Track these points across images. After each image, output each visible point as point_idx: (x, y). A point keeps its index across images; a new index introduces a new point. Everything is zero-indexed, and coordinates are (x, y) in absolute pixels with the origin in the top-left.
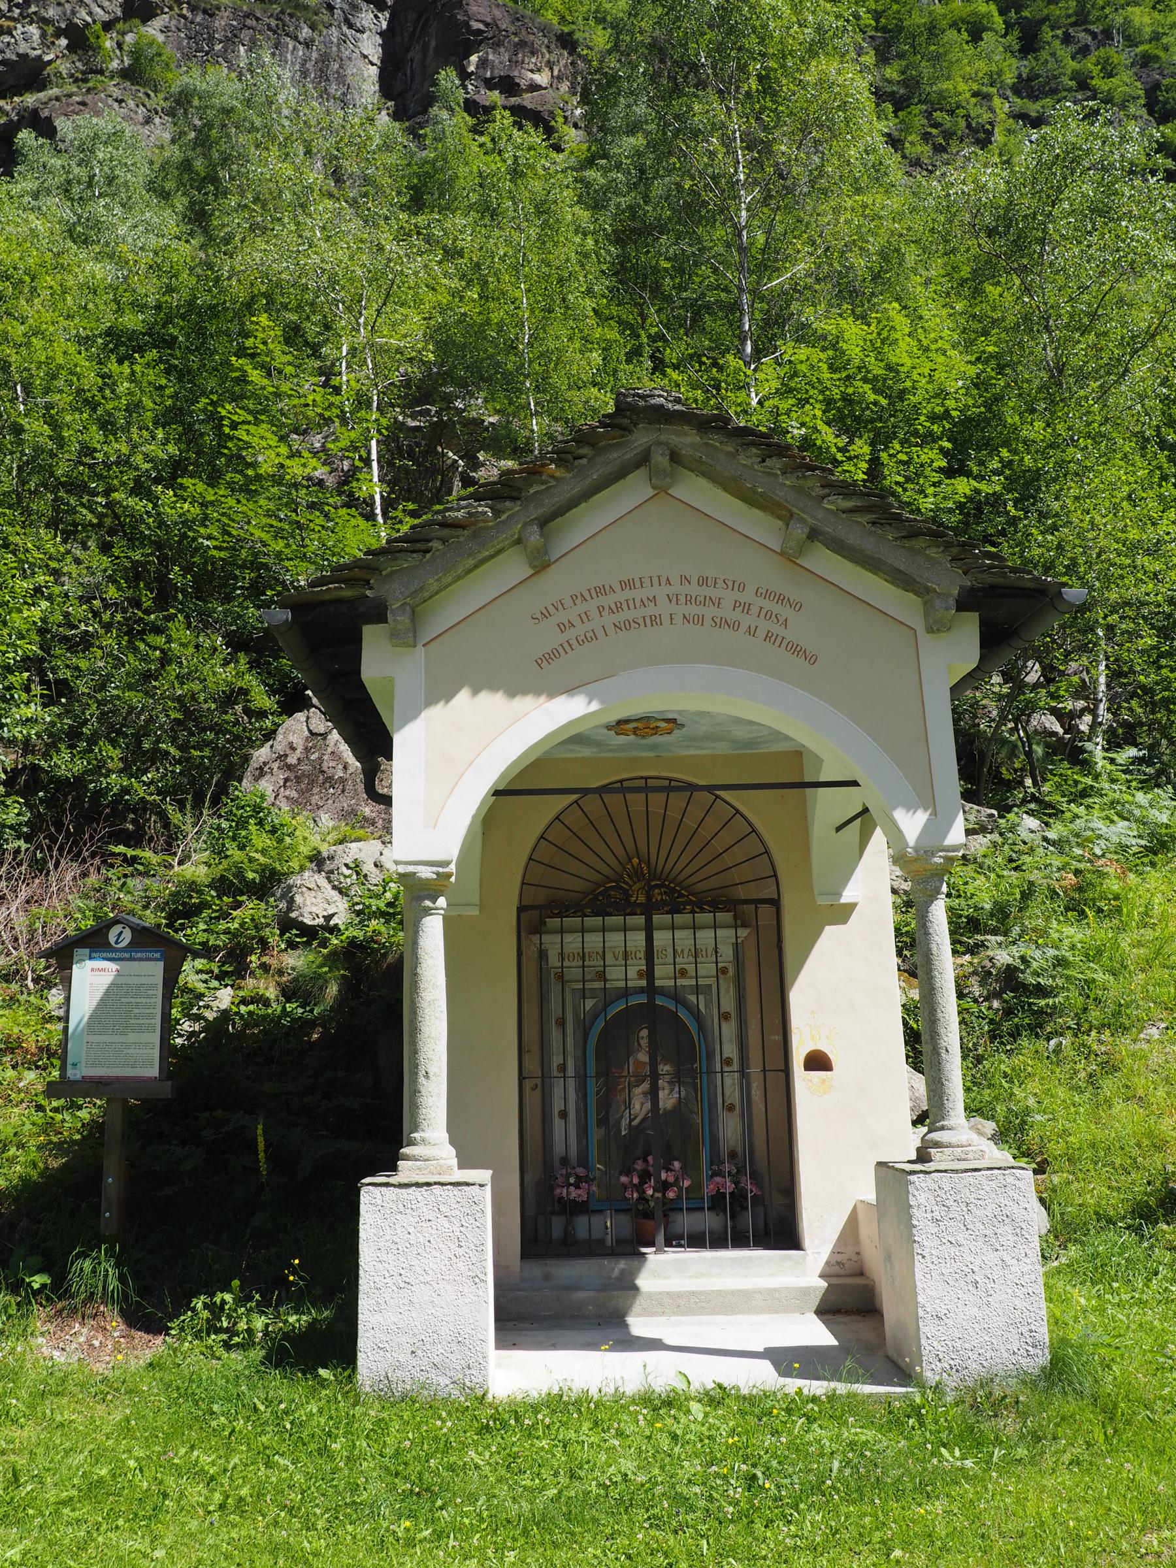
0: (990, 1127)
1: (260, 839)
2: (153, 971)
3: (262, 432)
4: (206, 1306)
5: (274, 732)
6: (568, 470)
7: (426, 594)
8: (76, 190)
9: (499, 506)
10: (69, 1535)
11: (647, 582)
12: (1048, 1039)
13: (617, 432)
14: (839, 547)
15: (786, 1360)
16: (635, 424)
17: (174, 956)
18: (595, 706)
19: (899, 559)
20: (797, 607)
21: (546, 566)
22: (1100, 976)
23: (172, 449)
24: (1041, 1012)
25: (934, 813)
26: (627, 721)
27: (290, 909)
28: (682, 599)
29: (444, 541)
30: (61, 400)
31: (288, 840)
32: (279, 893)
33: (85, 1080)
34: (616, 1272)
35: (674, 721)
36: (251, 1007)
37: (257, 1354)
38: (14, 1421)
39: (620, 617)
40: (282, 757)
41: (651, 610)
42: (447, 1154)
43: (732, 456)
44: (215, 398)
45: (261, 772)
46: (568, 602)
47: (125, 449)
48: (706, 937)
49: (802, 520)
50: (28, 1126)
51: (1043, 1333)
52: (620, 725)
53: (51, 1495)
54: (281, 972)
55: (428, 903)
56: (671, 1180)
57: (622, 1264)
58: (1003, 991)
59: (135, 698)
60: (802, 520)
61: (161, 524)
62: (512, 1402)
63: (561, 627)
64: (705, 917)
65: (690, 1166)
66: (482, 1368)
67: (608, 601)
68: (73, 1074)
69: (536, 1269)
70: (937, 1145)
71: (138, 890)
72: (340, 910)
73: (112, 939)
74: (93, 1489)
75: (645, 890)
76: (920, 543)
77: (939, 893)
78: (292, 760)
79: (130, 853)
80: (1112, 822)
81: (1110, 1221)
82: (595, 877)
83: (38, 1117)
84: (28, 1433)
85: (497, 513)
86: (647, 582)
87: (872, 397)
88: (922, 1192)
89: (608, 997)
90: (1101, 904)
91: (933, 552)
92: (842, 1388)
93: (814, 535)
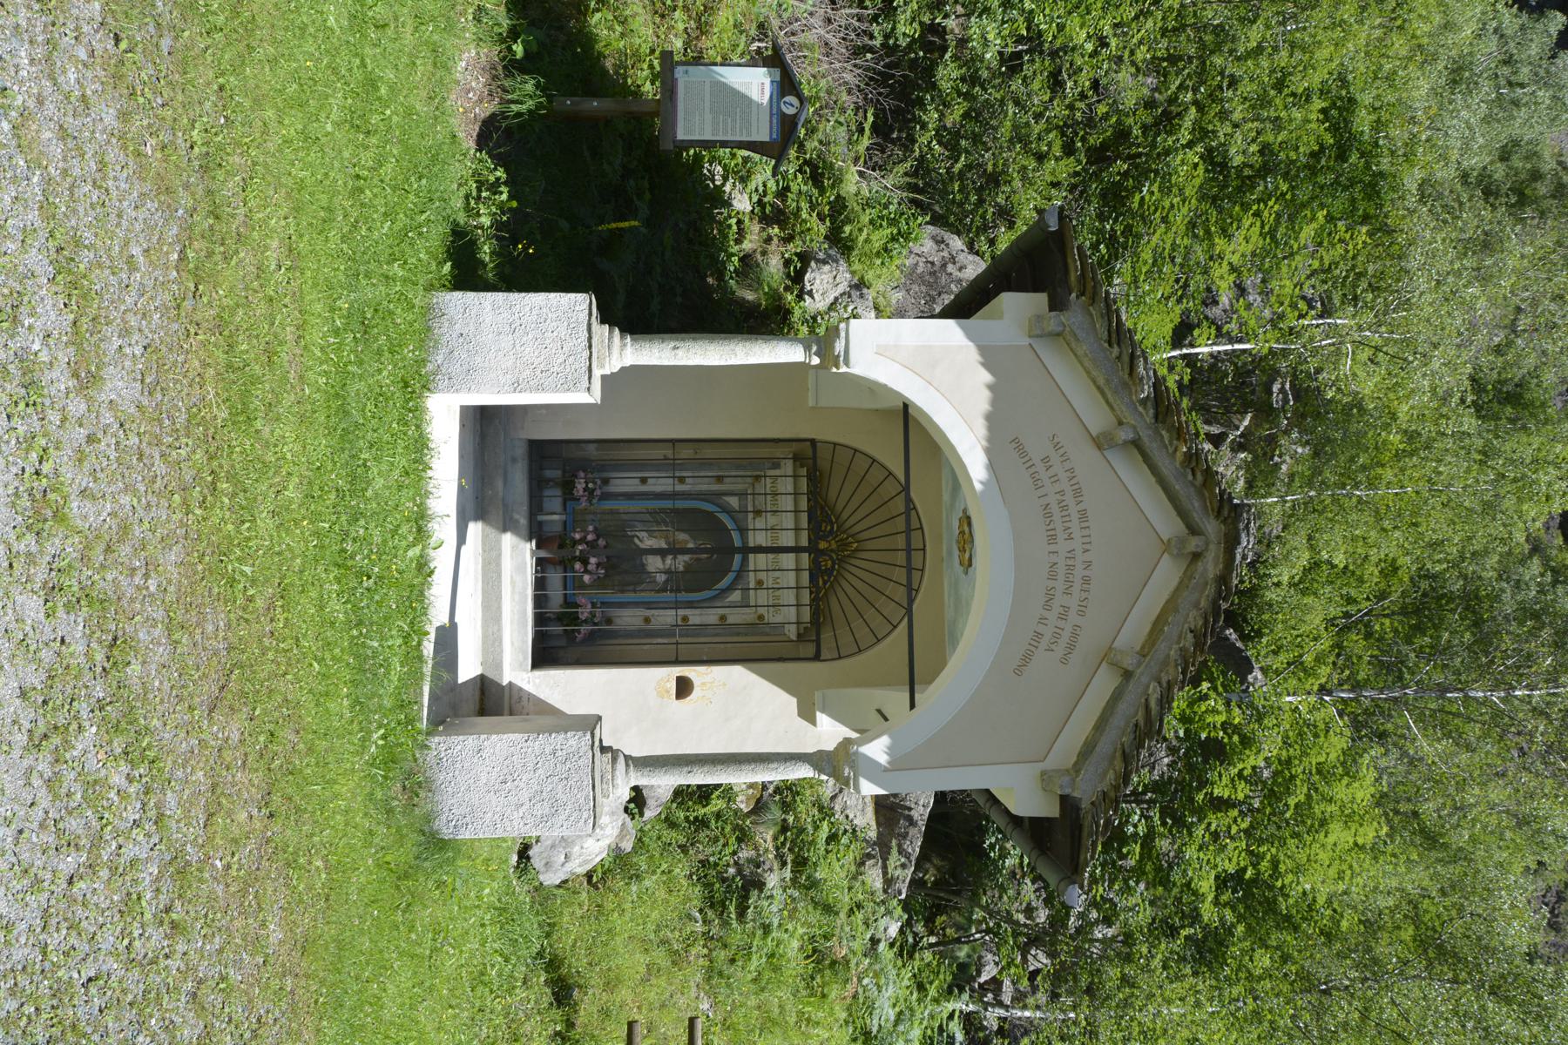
0: (628, 846)
1: (879, 238)
2: (762, 134)
3: (1254, 239)
4: (498, 179)
5: (977, 253)
6: (1182, 463)
7: (1073, 345)
8: (1506, 71)
9: (1149, 404)
10: (342, 62)
11: (1086, 532)
12: (701, 911)
13: (1216, 505)
14: (1116, 697)
15: (448, 638)
16: (1224, 521)
17: (775, 150)
18: (978, 487)
19: (1105, 746)
20: (1064, 661)
21: (1099, 447)
22: (755, 963)
23: (1238, 160)
24: (724, 907)
25: (886, 770)
26: (970, 524)
27: (818, 261)
28: (1070, 562)
29: (1119, 358)
30: (1283, 57)
31: (878, 262)
32: (832, 252)
33: (674, 82)
34: (516, 516)
35: (970, 565)
36: (735, 228)
37: (461, 218)
38: (416, 29)
39: (1055, 508)
40: (953, 260)
41: (1061, 536)
42: (614, 364)
43: (1196, 605)
44: (1288, 197)
45: (939, 242)
46: (1067, 465)
47: (1237, 116)
48: (789, 597)
49: (1139, 664)
50: (638, 41)
51: (465, 835)
52: (967, 520)
53: (368, 51)
54: (764, 253)
55: (814, 348)
56: (590, 567)
57: (523, 521)
58: (743, 877)
59: (1005, 130)
60: (1139, 664)
61: (1167, 152)
62: (424, 410)
63: (1046, 460)
64: (806, 597)
65: (599, 583)
66: (451, 388)
67: (1069, 499)
68: (679, 71)
69: (521, 451)
70: (614, 760)
71: (840, 138)
72: (817, 303)
73: (787, 99)
74: (371, 83)
75: (829, 547)
76: (1119, 765)
77: (821, 771)
78: (950, 268)
79: (867, 126)
80: (894, 1006)
81: (548, 935)
82: (839, 507)
83: (645, 49)
84: (408, 38)
85: (1144, 402)
86: (1086, 532)
87: (1292, 801)
88: (576, 742)
89: (738, 516)
90: (818, 979)
91: (1111, 775)
92: (428, 669)
93: (1127, 675)
